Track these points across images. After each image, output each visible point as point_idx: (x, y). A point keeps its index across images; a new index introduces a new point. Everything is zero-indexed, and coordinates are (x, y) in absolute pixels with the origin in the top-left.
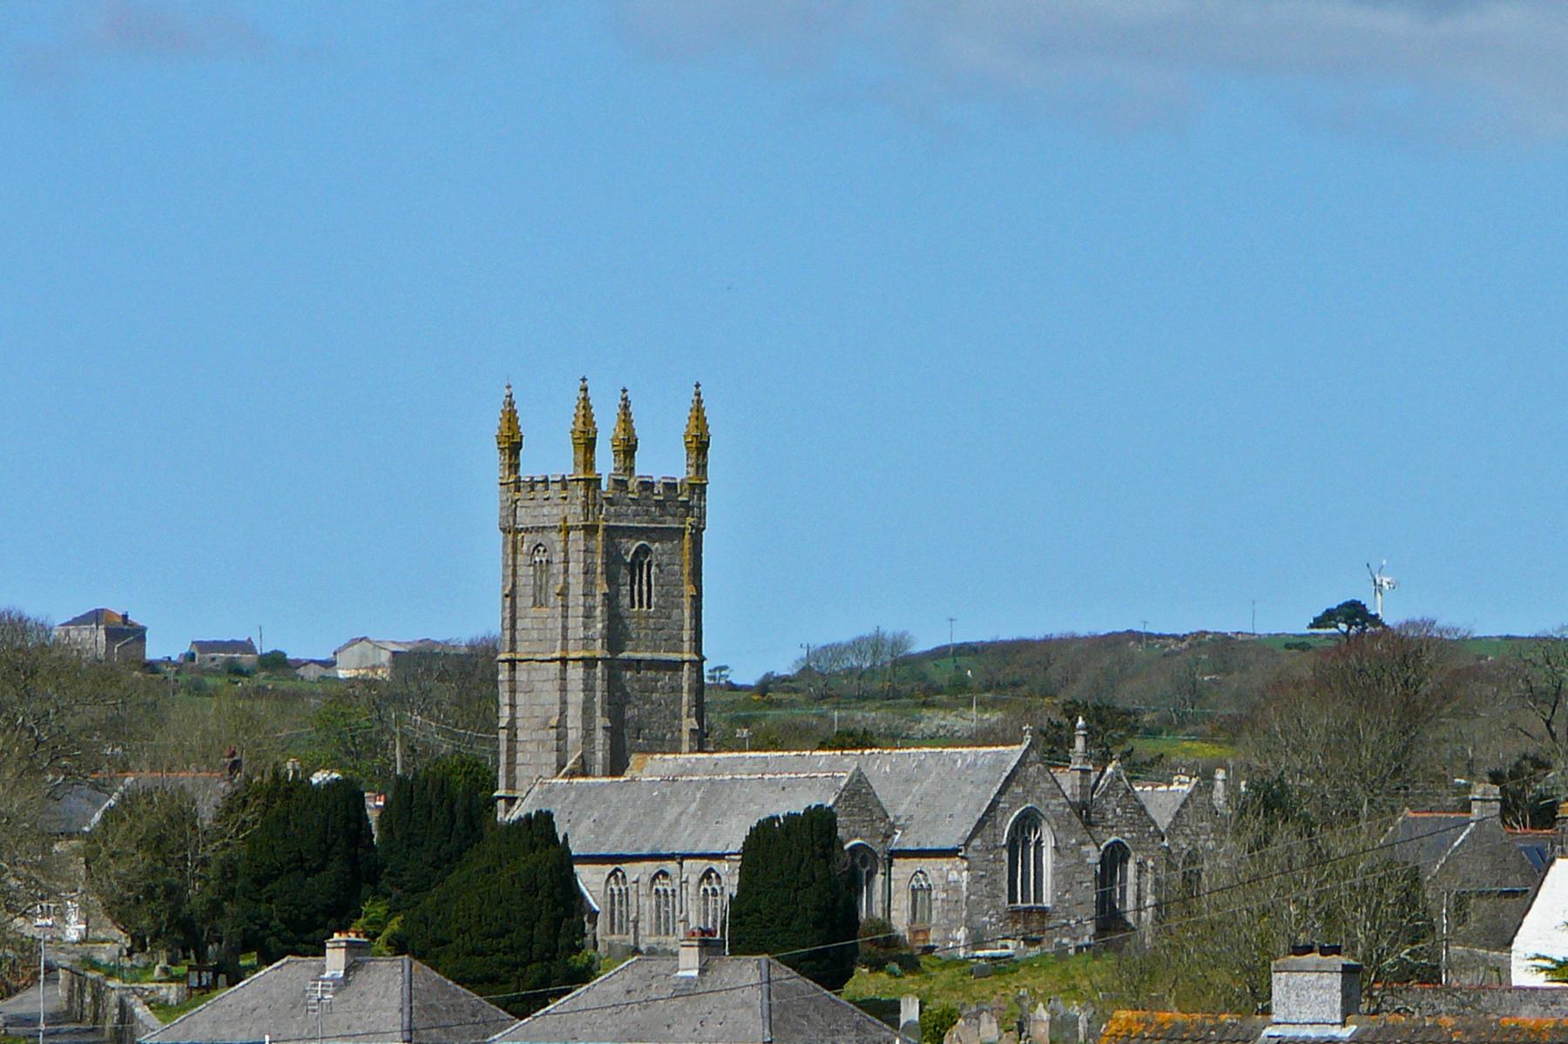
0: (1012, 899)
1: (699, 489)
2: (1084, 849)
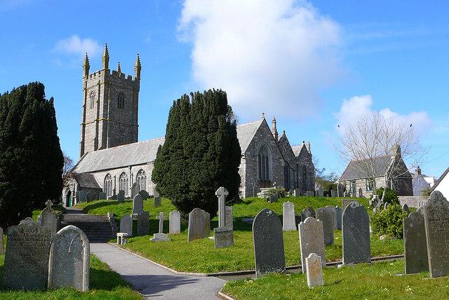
0: (260, 177)
1: (138, 79)
2: (281, 160)
